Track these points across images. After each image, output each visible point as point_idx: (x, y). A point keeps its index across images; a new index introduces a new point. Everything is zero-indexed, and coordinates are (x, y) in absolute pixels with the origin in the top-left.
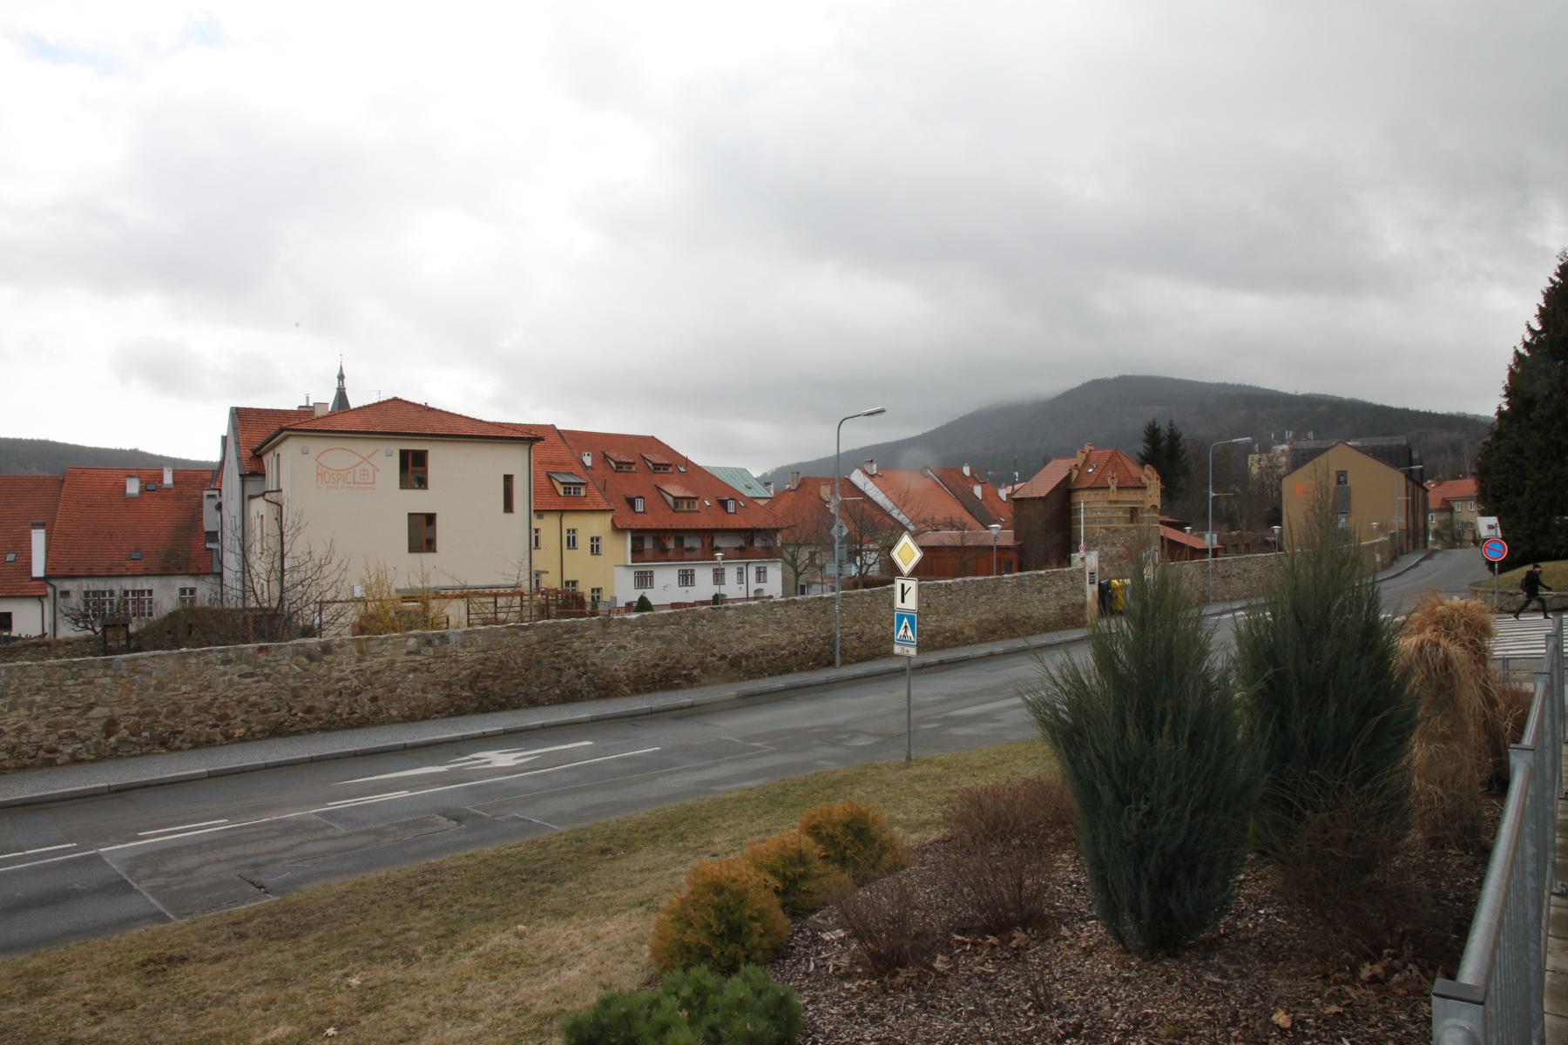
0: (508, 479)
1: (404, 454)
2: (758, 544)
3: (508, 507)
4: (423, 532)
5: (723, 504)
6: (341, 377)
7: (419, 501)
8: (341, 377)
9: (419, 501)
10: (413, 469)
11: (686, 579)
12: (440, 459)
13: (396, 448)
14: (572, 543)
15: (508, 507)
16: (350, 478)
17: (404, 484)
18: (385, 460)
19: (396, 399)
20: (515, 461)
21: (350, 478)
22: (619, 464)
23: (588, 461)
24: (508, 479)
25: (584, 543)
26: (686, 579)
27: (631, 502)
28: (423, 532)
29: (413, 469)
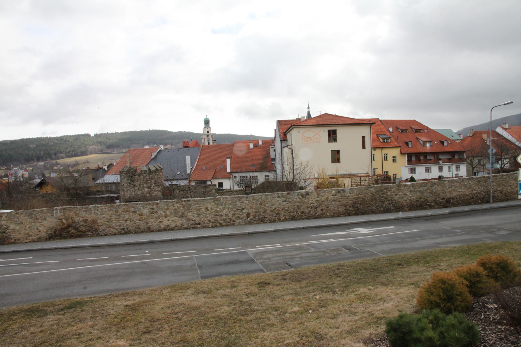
0: (363, 138)
1: (329, 131)
2: (456, 157)
3: (364, 147)
4: (336, 157)
5: (442, 143)
6: (309, 108)
7: (334, 146)
8: (309, 108)
9: (334, 146)
10: (332, 136)
11: (428, 170)
12: (341, 132)
13: (326, 129)
14: (386, 158)
15: (364, 147)
16: (313, 140)
17: (330, 141)
18: (324, 133)
19: (326, 114)
20: (366, 131)
21: (313, 140)
22: (402, 130)
23: (391, 130)
24: (363, 138)
25: (390, 158)
26: (428, 170)
27: (407, 144)
28: (336, 157)
29: (332, 136)
